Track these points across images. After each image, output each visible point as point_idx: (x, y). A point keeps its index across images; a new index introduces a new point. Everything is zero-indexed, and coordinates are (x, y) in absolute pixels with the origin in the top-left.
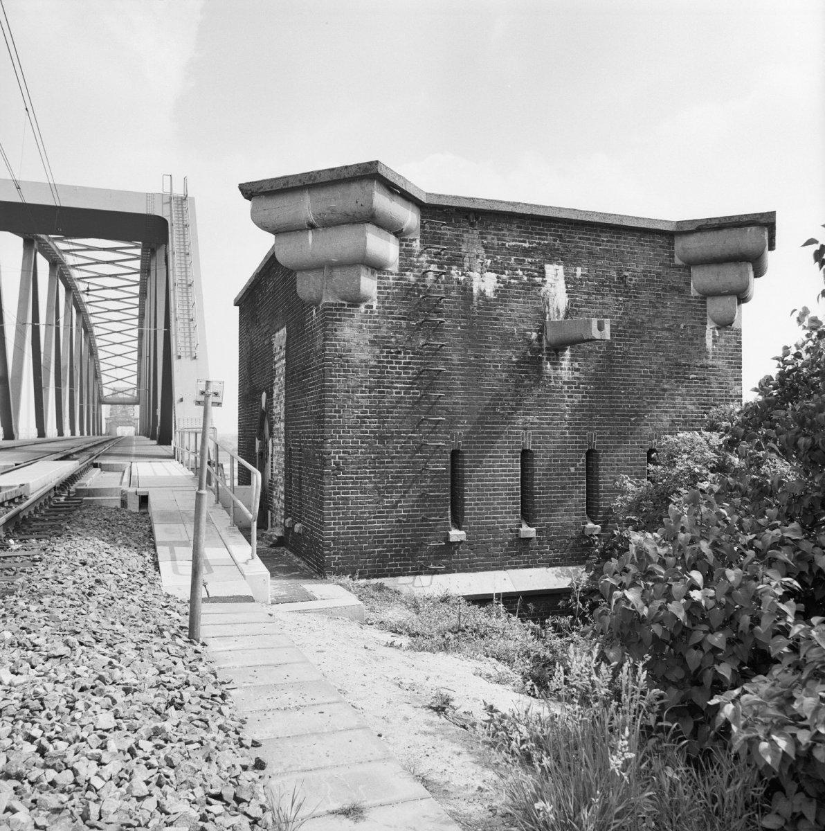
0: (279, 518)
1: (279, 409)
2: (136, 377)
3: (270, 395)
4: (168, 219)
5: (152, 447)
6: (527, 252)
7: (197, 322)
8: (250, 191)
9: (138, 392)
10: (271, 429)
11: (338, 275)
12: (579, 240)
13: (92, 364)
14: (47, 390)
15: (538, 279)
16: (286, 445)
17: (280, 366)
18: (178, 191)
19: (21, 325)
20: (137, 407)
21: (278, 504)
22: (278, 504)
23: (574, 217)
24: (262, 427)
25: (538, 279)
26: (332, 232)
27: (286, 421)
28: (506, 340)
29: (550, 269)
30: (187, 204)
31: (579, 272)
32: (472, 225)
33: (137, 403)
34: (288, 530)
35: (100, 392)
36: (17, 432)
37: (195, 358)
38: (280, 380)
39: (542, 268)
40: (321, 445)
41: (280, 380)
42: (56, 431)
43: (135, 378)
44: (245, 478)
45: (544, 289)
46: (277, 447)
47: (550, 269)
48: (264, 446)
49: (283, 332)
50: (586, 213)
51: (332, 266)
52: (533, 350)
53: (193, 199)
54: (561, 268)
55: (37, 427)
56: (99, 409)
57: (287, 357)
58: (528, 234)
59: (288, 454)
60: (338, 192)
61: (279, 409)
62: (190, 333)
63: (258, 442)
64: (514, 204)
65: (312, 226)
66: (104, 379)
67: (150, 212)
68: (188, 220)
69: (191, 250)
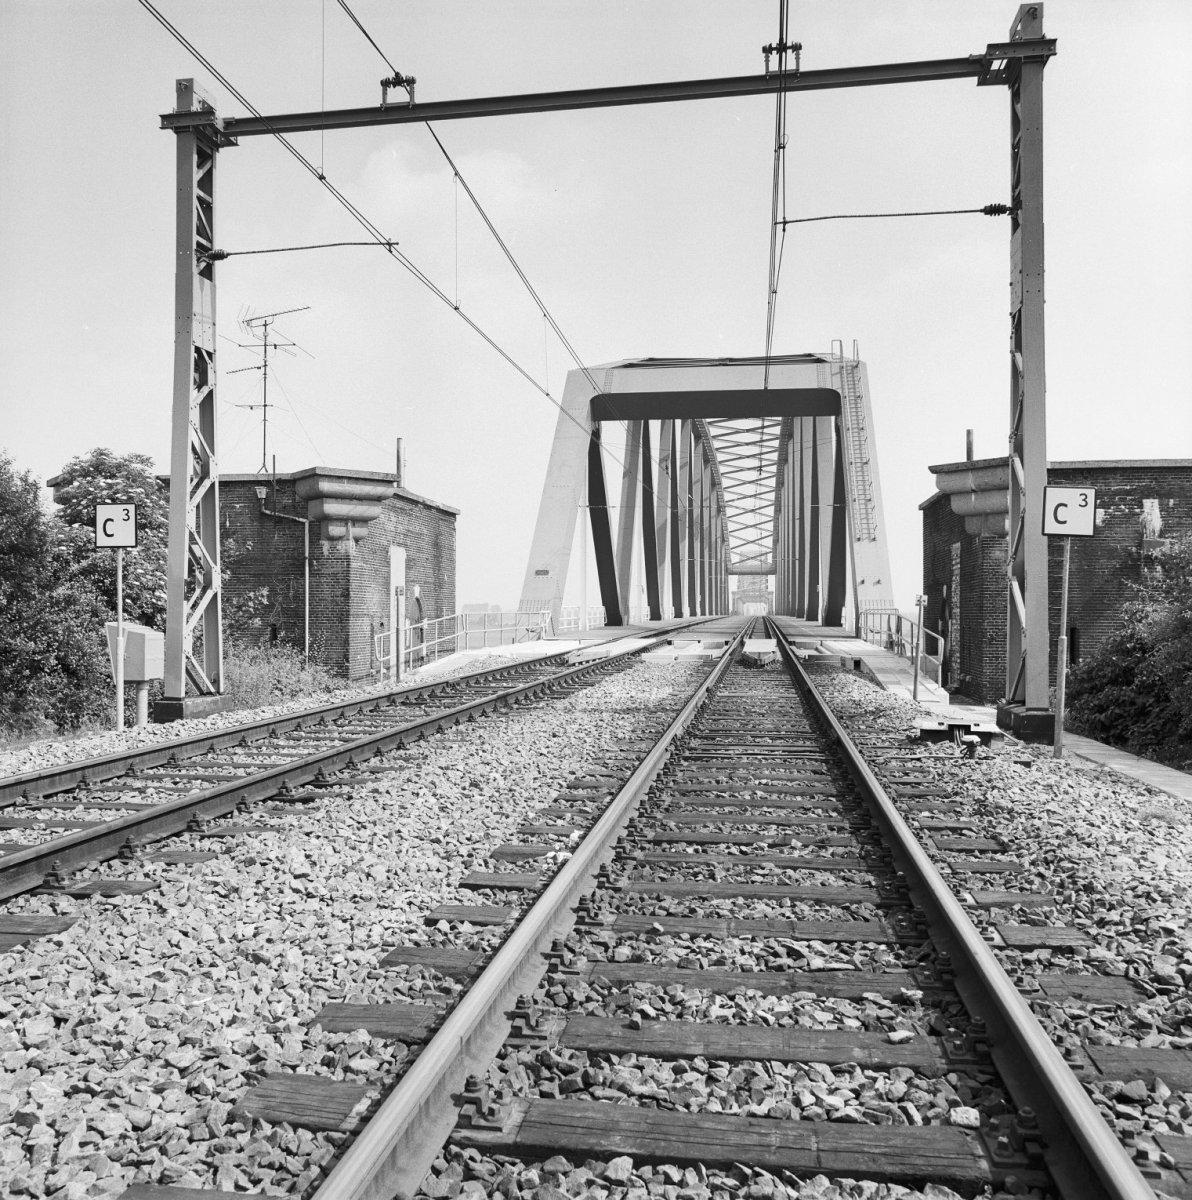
0: (957, 677)
1: (956, 599)
2: (771, 539)
3: (949, 588)
4: (840, 391)
5: (341, 682)
6: (1128, 493)
7: (875, 502)
8: (934, 470)
9: (774, 557)
10: (950, 612)
11: (991, 519)
12: (1172, 482)
13: (719, 523)
14: (663, 561)
15: (1138, 510)
16: (961, 625)
17: (957, 568)
18: (848, 355)
19: (629, 474)
20: (772, 579)
21: (956, 666)
22: (956, 666)
23: (1166, 465)
24: (944, 611)
25: (1138, 510)
26: (987, 494)
27: (961, 608)
28: (1112, 553)
29: (1147, 503)
30: (859, 373)
31: (1172, 502)
32: (1086, 478)
33: (773, 572)
34: (962, 682)
35: (727, 560)
36: (627, 611)
37: (874, 539)
38: (956, 579)
39: (1141, 502)
40: (981, 624)
41: (956, 579)
42: (646, 610)
43: (770, 539)
44: (931, 648)
45: (1142, 517)
46: (954, 626)
47: (1147, 503)
48: (945, 625)
49: (958, 545)
50: (1176, 461)
51: (987, 515)
52: (1133, 560)
53: (865, 364)
54: (1156, 501)
55: (604, 603)
56: (726, 581)
57: (961, 563)
58: (1130, 480)
59: (962, 630)
60: (989, 473)
61: (956, 599)
62: (867, 514)
63: (940, 623)
64: (1116, 462)
65: (973, 491)
66: (733, 542)
67: (822, 386)
68: (861, 391)
69: (866, 424)
